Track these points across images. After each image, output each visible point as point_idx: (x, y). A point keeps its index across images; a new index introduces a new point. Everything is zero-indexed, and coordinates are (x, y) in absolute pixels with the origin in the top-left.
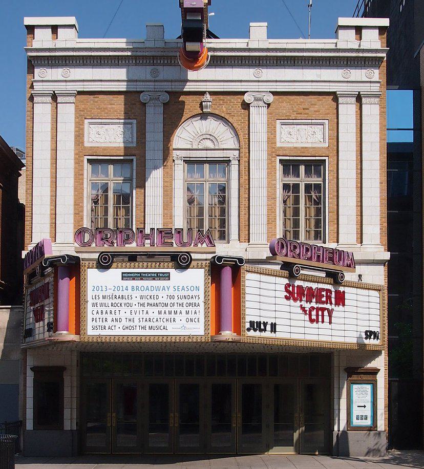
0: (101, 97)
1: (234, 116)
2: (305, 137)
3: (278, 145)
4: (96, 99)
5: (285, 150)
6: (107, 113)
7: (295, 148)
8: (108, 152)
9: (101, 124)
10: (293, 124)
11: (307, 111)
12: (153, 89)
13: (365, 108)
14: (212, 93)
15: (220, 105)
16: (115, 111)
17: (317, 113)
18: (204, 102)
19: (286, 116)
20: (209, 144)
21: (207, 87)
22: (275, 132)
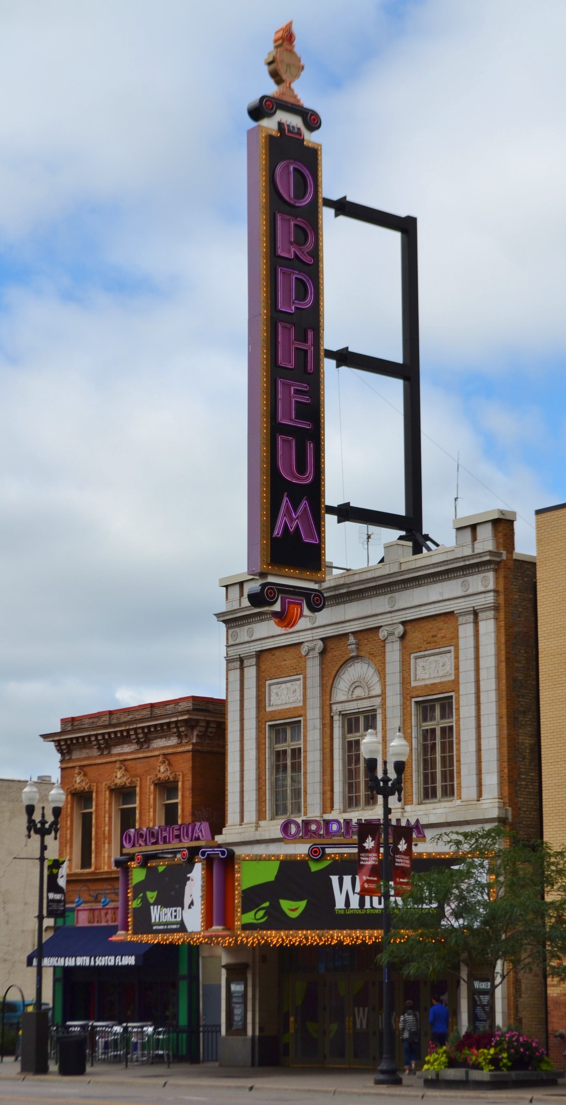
0: (277, 653)
1: (376, 656)
2: (431, 670)
3: (413, 684)
4: (274, 657)
5: (417, 690)
6: (281, 671)
7: (426, 686)
8: (273, 717)
9: (278, 683)
10: (425, 656)
11: (435, 639)
12: (311, 639)
13: (482, 625)
14: (353, 633)
15: (365, 645)
16: (287, 668)
17: (444, 639)
18: (350, 645)
19: (419, 648)
20: (359, 692)
21: (352, 627)
22: (410, 669)
